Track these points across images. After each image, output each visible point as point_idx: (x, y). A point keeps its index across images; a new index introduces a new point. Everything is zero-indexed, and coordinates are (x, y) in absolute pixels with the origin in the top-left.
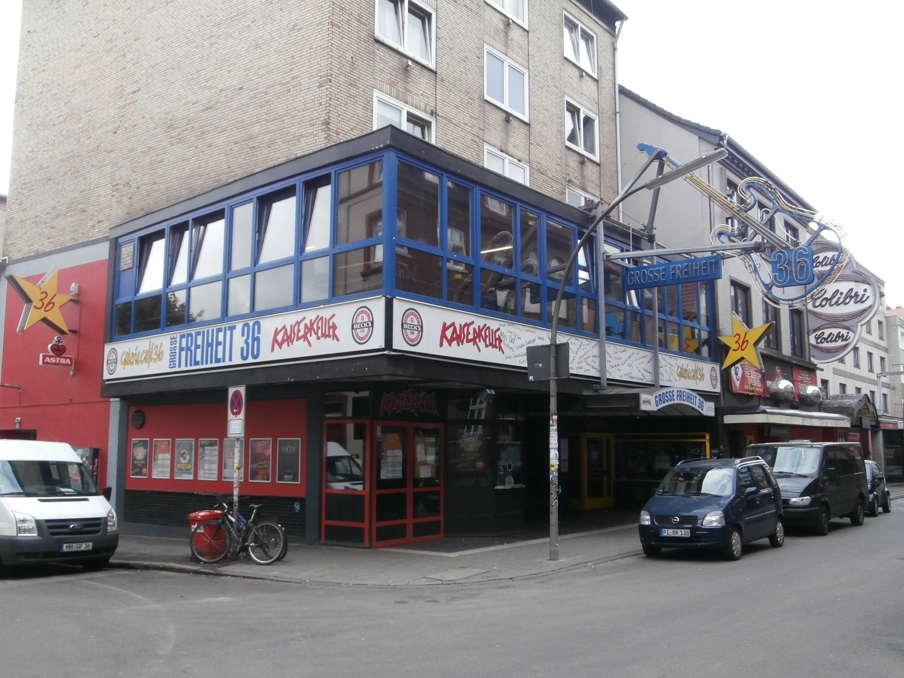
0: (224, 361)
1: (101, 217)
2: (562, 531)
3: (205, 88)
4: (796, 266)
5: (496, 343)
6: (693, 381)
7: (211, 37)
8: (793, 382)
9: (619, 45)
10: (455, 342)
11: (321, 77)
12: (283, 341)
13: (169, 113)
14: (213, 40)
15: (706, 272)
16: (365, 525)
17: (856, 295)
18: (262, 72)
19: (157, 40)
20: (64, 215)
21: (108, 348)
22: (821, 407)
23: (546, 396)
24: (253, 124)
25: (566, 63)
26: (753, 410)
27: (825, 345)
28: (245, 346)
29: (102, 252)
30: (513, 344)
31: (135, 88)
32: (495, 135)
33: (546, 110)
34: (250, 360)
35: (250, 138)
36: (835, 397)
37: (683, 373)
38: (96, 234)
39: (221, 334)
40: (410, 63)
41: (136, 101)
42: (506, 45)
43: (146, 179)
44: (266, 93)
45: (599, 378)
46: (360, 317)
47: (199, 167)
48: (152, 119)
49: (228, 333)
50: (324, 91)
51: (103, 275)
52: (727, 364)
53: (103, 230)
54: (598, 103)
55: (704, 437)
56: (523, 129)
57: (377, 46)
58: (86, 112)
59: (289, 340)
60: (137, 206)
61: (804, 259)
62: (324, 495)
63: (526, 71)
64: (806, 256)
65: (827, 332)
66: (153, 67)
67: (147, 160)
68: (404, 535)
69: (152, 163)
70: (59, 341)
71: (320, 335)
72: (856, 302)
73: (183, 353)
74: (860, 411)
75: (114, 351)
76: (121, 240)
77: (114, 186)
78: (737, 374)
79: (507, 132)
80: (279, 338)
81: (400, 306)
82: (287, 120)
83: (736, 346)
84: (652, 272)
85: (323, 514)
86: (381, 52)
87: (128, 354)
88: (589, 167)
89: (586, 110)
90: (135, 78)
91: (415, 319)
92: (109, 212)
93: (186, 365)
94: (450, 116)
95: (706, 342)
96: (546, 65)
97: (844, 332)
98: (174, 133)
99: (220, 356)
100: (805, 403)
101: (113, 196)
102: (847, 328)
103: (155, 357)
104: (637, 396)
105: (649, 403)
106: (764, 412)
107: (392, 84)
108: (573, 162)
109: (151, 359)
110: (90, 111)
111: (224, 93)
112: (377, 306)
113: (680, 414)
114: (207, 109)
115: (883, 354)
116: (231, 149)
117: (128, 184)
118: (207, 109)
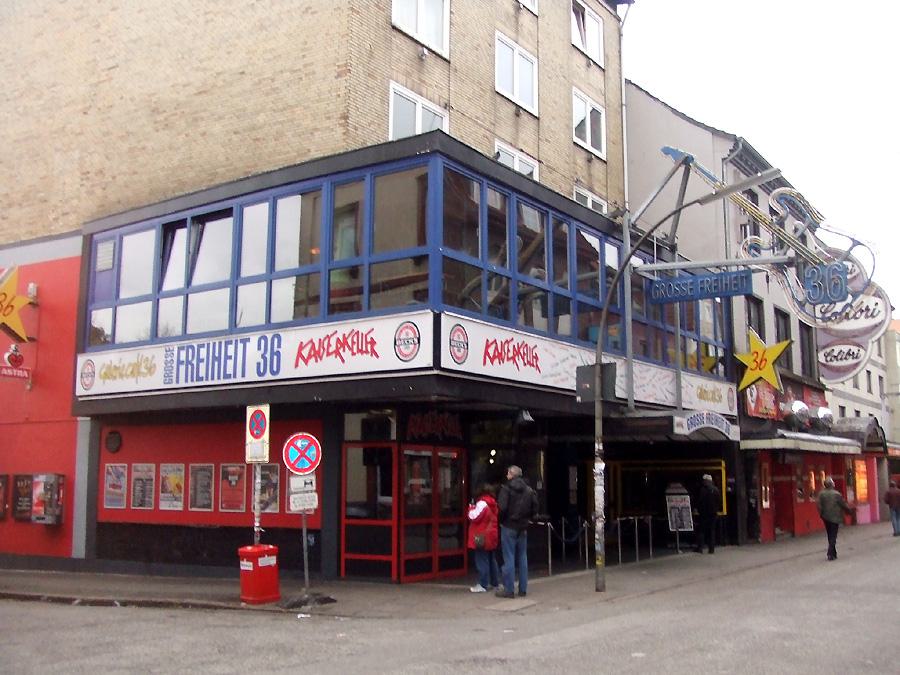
0: (235, 376)
1: (67, 208)
2: (640, 559)
3: (197, 69)
4: (829, 284)
5: (533, 362)
6: (132, 380)
7: (206, 13)
8: (807, 404)
9: (624, 31)
10: (313, 359)
11: (338, 66)
12: (310, 356)
13: (154, 94)
14: (209, 17)
15: (731, 285)
16: (393, 558)
17: (867, 309)
18: (269, 56)
19: (140, 11)
20: (20, 205)
21: (81, 359)
22: (830, 432)
23: (592, 419)
24: (258, 113)
25: (575, 52)
26: (770, 435)
27: (835, 363)
28: (262, 361)
29: (73, 248)
30: (555, 364)
31: (111, 63)
32: (505, 130)
33: (555, 103)
34: (268, 376)
35: (253, 128)
36: (851, 420)
37: (702, 395)
38: (59, 228)
39: (231, 348)
40: (426, 51)
41: (111, 79)
42: (517, 31)
43: (124, 168)
44: (273, 80)
45: (626, 400)
46: (404, 332)
47: (191, 158)
48: (132, 100)
49: (240, 346)
50: (342, 82)
51: (74, 276)
52: (741, 387)
53: (73, 222)
54: (605, 95)
55: (720, 464)
56: (532, 123)
57: (394, 33)
58: (48, 88)
59: (316, 355)
60: (113, 198)
61: (830, 279)
62: (343, 528)
63: (535, 60)
64: (839, 272)
65: (837, 349)
66: (135, 41)
67: (125, 146)
68: (429, 570)
69: (131, 150)
70: (16, 350)
71: (355, 351)
72: (867, 317)
73: (182, 368)
74: (870, 436)
75: (90, 363)
76: (95, 236)
77: (84, 174)
78: (752, 396)
79: (517, 126)
80: (305, 353)
81: (447, 322)
82: (298, 111)
83: (754, 365)
84: (678, 285)
85: (343, 548)
86: (398, 40)
87: (109, 367)
88: (597, 164)
89: (594, 103)
90: (112, 53)
91: (410, 332)
92: (76, 202)
93: (186, 381)
94: (463, 110)
95: (722, 360)
96: (555, 53)
97: (854, 349)
98: (160, 118)
99: (230, 371)
100: (816, 426)
101: (82, 185)
102: (859, 345)
103: (145, 371)
104: (670, 419)
105: (682, 428)
106: (783, 437)
107: (408, 74)
108: (581, 159)
109: (139, 373)
110: (54, 85)
111: (221, 77)
112: (424, 320)
113: (704, 438)
114: (200, 93)
115: (882, 373)
116: (230, 140)
117: (101, 172)
118: (200, 93)
